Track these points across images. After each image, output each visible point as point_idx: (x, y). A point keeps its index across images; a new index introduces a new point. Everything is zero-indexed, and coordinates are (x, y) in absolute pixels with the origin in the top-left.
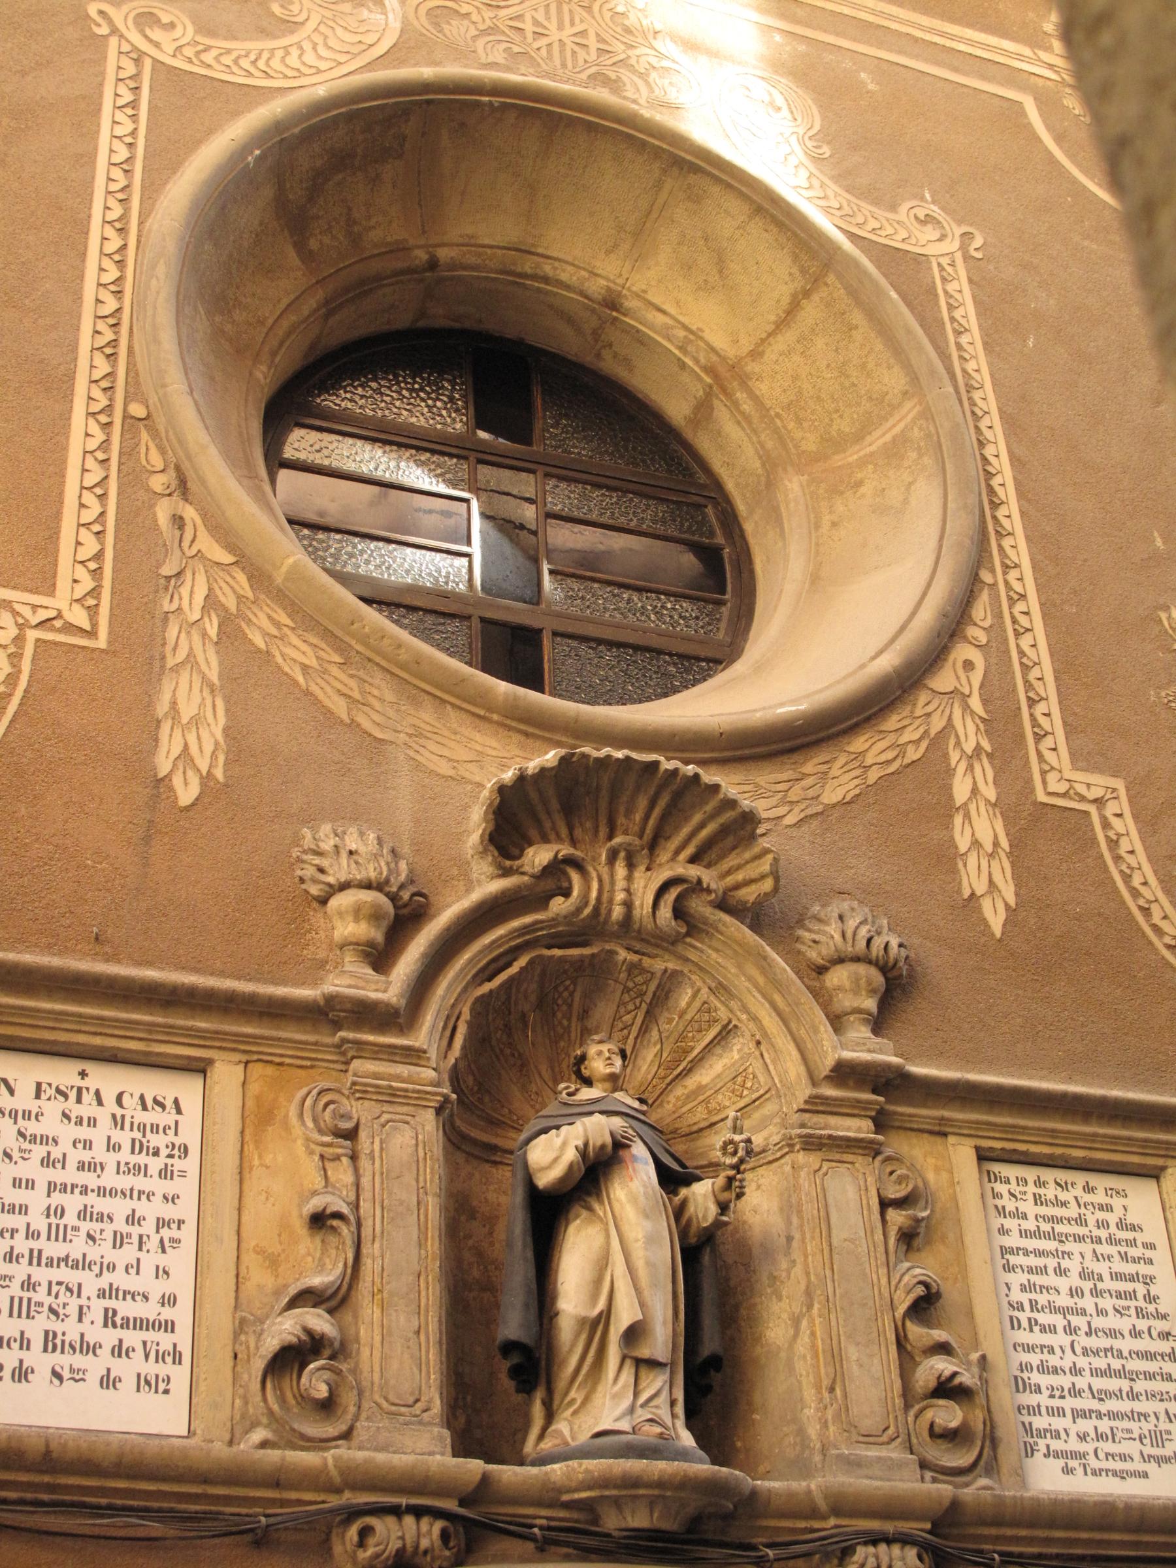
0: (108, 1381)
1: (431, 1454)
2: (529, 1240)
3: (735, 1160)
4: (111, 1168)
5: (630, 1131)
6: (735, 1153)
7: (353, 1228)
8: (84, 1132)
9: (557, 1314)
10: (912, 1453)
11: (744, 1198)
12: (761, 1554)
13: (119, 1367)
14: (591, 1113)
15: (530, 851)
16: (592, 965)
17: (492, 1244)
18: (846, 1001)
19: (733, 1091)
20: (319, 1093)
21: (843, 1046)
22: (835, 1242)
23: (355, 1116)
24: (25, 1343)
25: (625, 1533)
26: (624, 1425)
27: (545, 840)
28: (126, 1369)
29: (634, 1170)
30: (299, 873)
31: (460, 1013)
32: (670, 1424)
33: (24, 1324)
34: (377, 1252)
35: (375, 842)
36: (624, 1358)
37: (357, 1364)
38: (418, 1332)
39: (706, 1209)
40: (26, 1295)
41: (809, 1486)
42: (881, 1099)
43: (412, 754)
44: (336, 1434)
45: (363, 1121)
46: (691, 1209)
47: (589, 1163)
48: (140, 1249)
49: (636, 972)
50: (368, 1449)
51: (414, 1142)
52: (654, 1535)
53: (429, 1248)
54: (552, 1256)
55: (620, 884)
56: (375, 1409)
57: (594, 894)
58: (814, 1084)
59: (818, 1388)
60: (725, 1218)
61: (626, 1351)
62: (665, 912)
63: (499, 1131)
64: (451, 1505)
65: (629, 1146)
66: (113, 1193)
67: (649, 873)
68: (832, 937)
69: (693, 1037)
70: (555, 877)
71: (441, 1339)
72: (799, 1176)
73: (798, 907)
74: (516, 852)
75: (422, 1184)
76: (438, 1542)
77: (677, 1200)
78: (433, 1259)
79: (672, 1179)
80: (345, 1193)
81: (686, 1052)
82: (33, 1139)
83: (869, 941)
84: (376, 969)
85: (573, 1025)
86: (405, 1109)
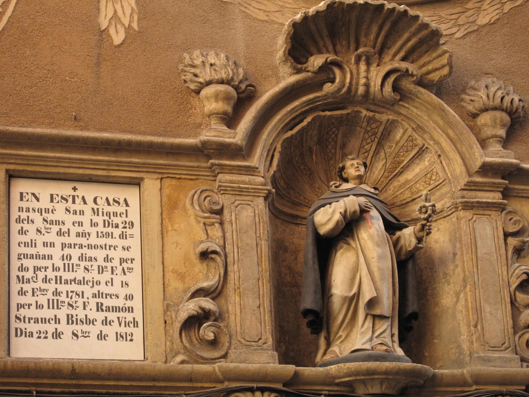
0: (101, 337)
3: (426, 215)
4: (94, 235)
6: (426, 212)
7: (223, 258)
8: (78, 218)
9: (332, 296)
10: (517, 354)
11: (431, 235)
13: (106, 330)
14: (348, 196)
15: (312, 59)
18: (488, 132)
20: (201, 192)
22: (479, 255)
24: (57, 321)
26: (368, 346)
27: (320, 52)
28: (110, 331)
29: (372, 223)
30: (183, 77)
32: (391, 345)
35: (225, 58)
36: (367, 315)
37: (228, 323)
39: (411, 241)
40: (55, 298)
42: (507, 182)
43: (243, 9)
44: (219, 356)
45: (225, 205)
46: (402, 242)
47: (346, 221)
48: (112, 273)
49: (372, 122)
50: (235, 362)
51: (253, 214)
53: (263, 266)
55: (363, 74)
57: (348, 80)
58: (470, 175)
59: (469, 325)
60: (420, 245)
62: (388, 88)
63: (298, 208)
64: (279, 386)
65: (369, 211)
66: (96, 247)
67: (379, 68)
68: (482, 97)
69: (403, 155)
73: (463, 82)
75: (258, 235)
77: (395, 237)
79: (392, 227)
80: (217, 241)
81: (400, 163)
82: (52, 223)
83: (502, 99)
84: (229, 126)
86: (248, 198)
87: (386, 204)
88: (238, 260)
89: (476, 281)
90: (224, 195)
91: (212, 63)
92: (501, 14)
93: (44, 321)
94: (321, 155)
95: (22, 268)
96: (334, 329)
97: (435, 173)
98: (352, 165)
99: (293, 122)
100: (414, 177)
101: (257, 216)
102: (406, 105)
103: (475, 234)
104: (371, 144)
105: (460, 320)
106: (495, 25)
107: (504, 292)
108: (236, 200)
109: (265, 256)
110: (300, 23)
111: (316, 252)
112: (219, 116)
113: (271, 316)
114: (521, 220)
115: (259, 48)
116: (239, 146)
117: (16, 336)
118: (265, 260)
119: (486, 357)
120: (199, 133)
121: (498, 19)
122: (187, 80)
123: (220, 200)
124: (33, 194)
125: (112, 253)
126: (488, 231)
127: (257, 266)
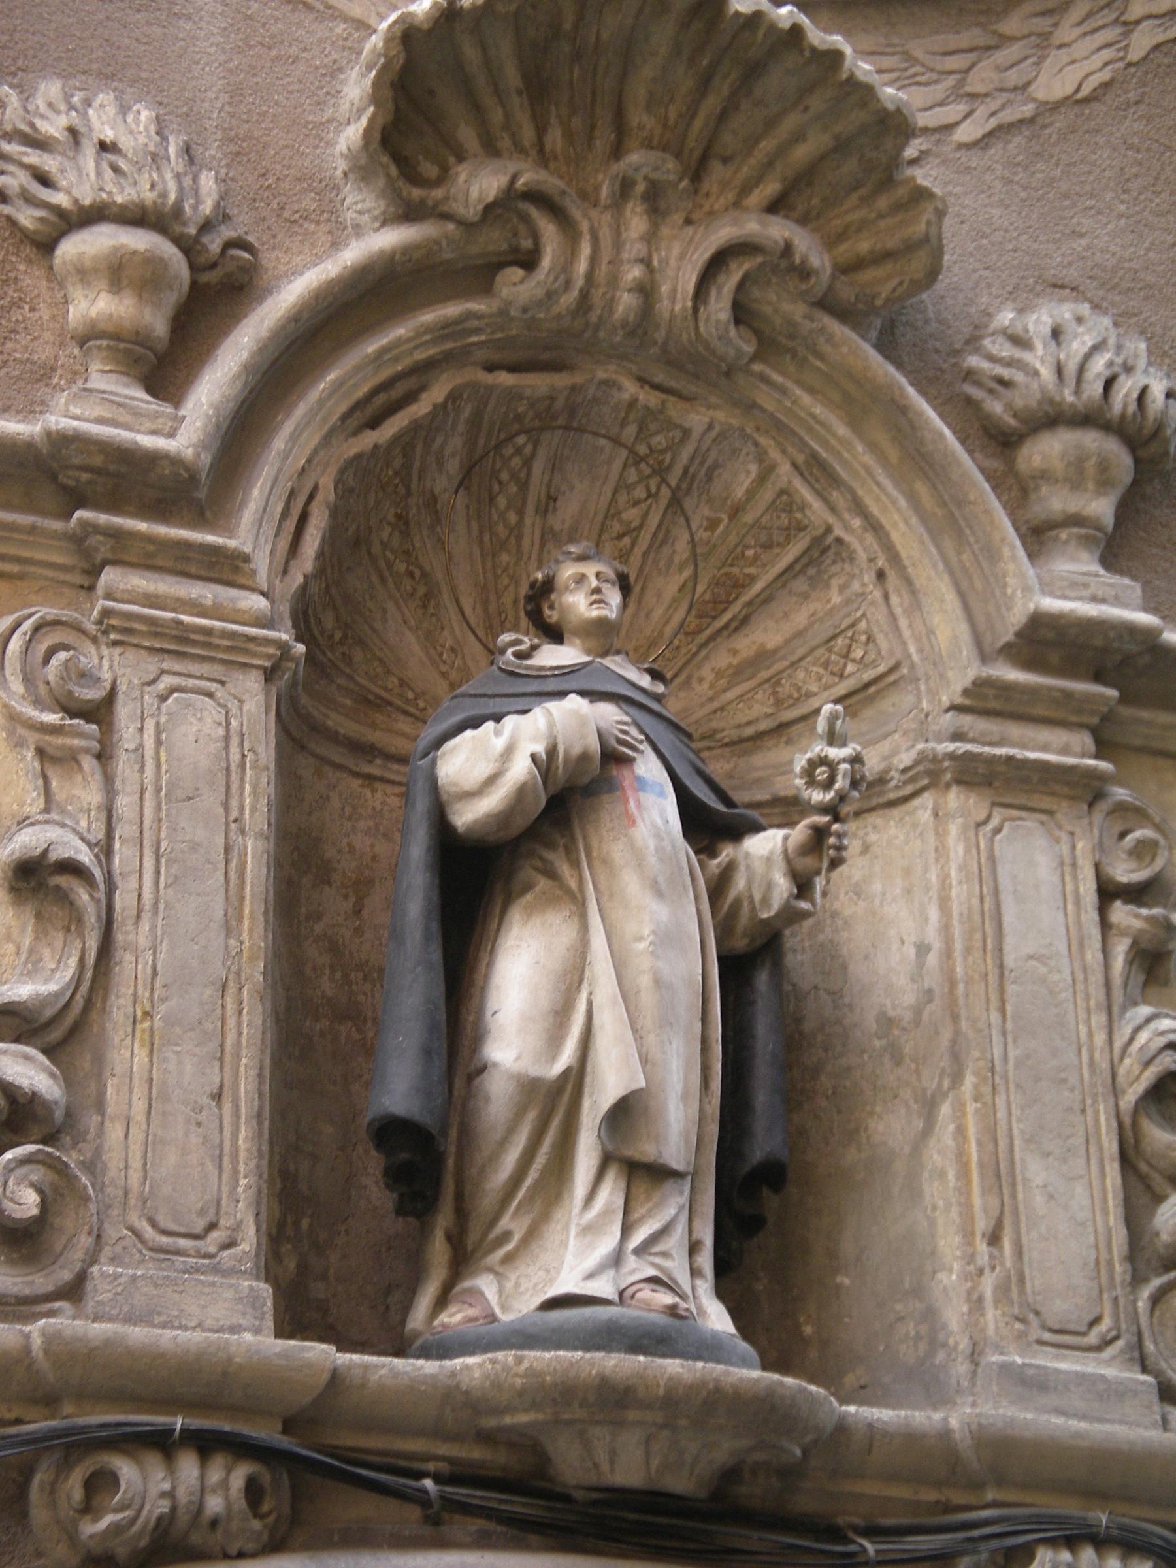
1: (234, 1329)
2: (435, 926)
3: (830, 795)
5: (634, 732)
6: (831, 781)
7: (101, 895)
9: (482, 1069)
10: (1144, 1370)
11: (843, 869)
12: (852, 1548)
14: (562, 694)
15: (462, 172)
16: (572, 410)
17: (358, 931)
18: (1056, 501)
19: (826, 665)
20: (37, 629)
21: (1048, 588)
22: (1009, 961)
23: (106, 676)
25: (595, 1495)
26: (603, 1287)
27: (491, 149)
29: (639, 805)
31: (316, 488)
32: (687, 1289)
34: (143, 941)
35: (153, 129)
36: (606, 1161)
37: (98, 1151)
38: (218, 1097)
39: (770, 886)
41: (945, 1419)
42: (1113, 693)
44: (50, 1288)
45: (122, 687)
46: (740, 883)
47: (552, 792)
50: (111, 1319)
51: (221, 731)
52: (652, 1501)
53: (245, 936)
54: (476, 959)
55: (634, 248)
56: (131, 1239)
57: (582, 267)
58: (984, 658)
59: (968, 1235)
60: (804, 905)
61: (610, 1147)
62: (719, 308)
63: (379, 718)
64: (267, 1432)
65: (630, 761)
67: (689, 230)
68: (1036, 373)
69: (756, 557)
70: (504, 241)
71: (261, 1108)
72: (946, 832)
73: (973, 310)
74: (430, 170)
75: (234, 814)
76: (240, 1504)
77: (715, 864)
78: (252, 959)
79: (710, 825)
80: (84, 824)
81: (740, 585)
83: (1109, 384)
84: (152, 390)
85: (528, 521)
86: (205, 669)
87: (689, 736)
88: (156, 905)
89: (997, 1062)
90: (118, 650)
91: (108, 138)
92: (1121, 65)
94: (469, 527)
96: (487, 1202)
97: (863, 638)
98: (581, 579)
99: (381, 399)
100: (787, 642)
101: (235, 741)
102: (777, 378)
103: (995, 880)
104: (644, 506)
105: (934, 1208)
106: (1095, 105)
107: (1097, 1113)
108: (163, 672)
109: (252, 896)
110: (430, 32)
111: (436, 899)
112: (122, 346)
113: (260, 1134)
114: (1162, 842)
115: (277, 103)
116: (187, 469)
118: (252, 912)
119: (1031, 1372)
120: (43, 403)
121: (1106, 85)
122: (9, 192)
123: (106, 664)
126: (1043, 873)
127: (223, 935)
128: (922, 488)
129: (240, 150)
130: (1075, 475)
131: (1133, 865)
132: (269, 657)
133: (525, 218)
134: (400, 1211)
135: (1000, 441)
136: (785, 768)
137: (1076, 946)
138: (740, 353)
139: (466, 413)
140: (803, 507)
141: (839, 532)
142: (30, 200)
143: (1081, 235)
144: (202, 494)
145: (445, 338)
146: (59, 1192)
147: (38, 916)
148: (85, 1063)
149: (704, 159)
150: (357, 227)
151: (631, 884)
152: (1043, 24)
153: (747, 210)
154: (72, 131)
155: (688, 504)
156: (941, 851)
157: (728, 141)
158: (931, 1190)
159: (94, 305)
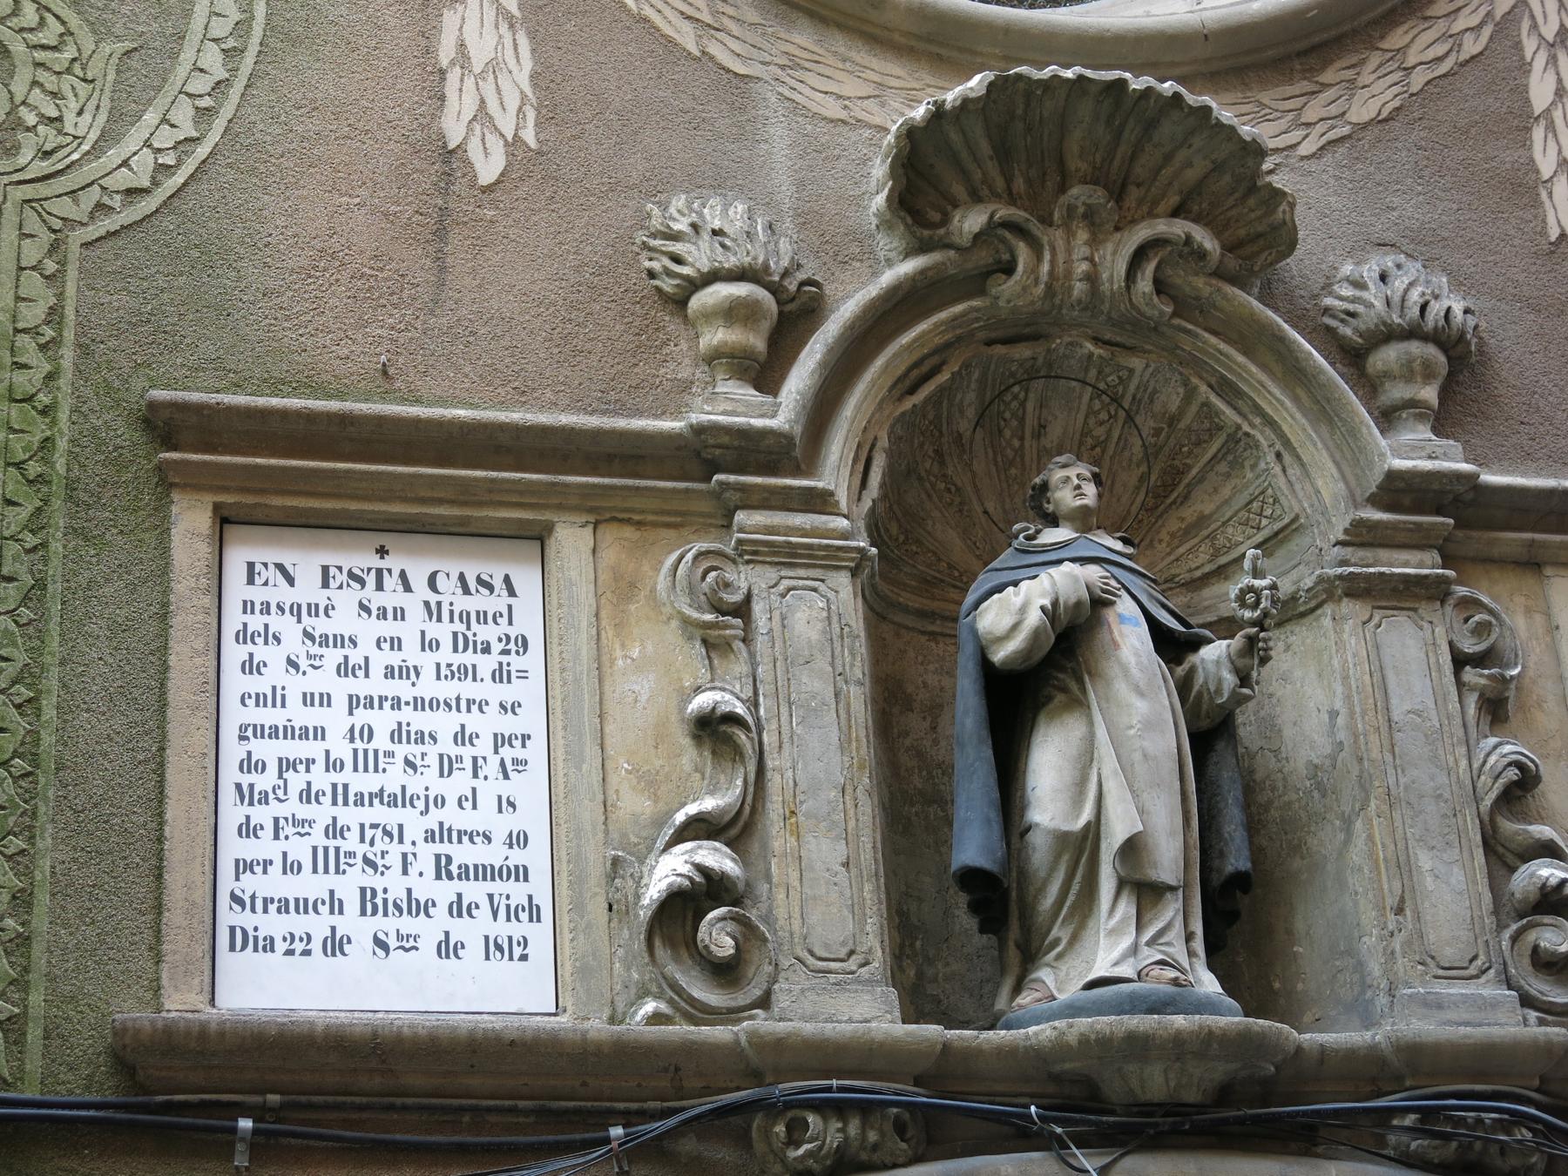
4: (428, 672)
5: (1113, 583)
6: (1258, 603)
8: (389, 628)
10: (1510, 988)
13: (461, 929)
17: (936, 742)
18: (1397, 392)
20: (696, 558)
23: (744, 585)
24: (336, 906)
26: (1126, 970)
27: (976, 198)
29: (1121, 634)
32: (1186, 965)
33: (332, 880)
37: (770, 910)
39: (1220, 681)
40: (332, 843)
41: (1373, 1037)
42: (1452, 521)
46: (1199, 680)
51: (825, 614)
57: (1045, 267)
62: (1144, 284)
66: (434, 704)
67: (1118, 235)
68: (1371, 306)
69: (1190, 452)
79: (1172, 646)
81: (1181, 473)
82: (324, 641)
83: (1424, 308)
84: (759, 387)
93: (304, 906)
95: (250, 764)
100: (1218, 508)
101: (835, 619)
110: (926, 128)
117: (232, 948)
121: (1397, 109)
124: (280, 567)
125: (473, 721)
128: (1300, 392)
129: (805, 219)
130: (1408, 373)
131: (1474, 641)
132: (852, 559)
133: (1003, 240)
134: (982, 931)
135: (1352, 357)
136: (1224, 597)
137: (1439, 699)
138: (1162, 313)
139: (976, 375)
140: (1218, 413)
141: (1246, 428)
142: (669, 273)
143: (1394, 209)
144: (798, 452)
145: (954, 328)
146: (748, 934)
147: (714, 753)
148: (755, 847)
149: (1124, 186)
150: (888, 260)
151: (1121, 688)
152: (1349, 74)
153: (1157, 216)
154: (694, 226)
155: (1139, 420)
156: (1340, 644)
157: (1139, 171)
158: (1353, 881)
159: (717, 336)
